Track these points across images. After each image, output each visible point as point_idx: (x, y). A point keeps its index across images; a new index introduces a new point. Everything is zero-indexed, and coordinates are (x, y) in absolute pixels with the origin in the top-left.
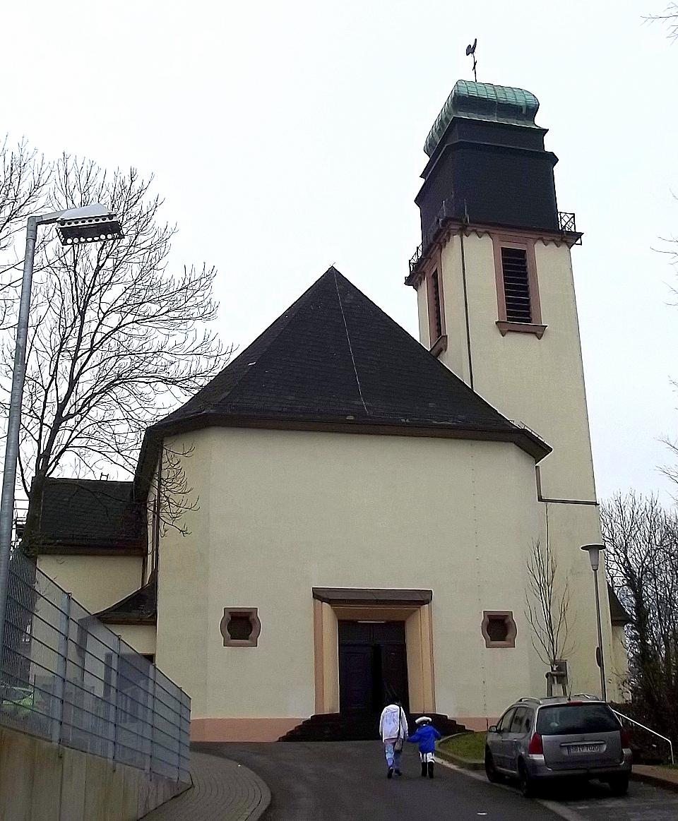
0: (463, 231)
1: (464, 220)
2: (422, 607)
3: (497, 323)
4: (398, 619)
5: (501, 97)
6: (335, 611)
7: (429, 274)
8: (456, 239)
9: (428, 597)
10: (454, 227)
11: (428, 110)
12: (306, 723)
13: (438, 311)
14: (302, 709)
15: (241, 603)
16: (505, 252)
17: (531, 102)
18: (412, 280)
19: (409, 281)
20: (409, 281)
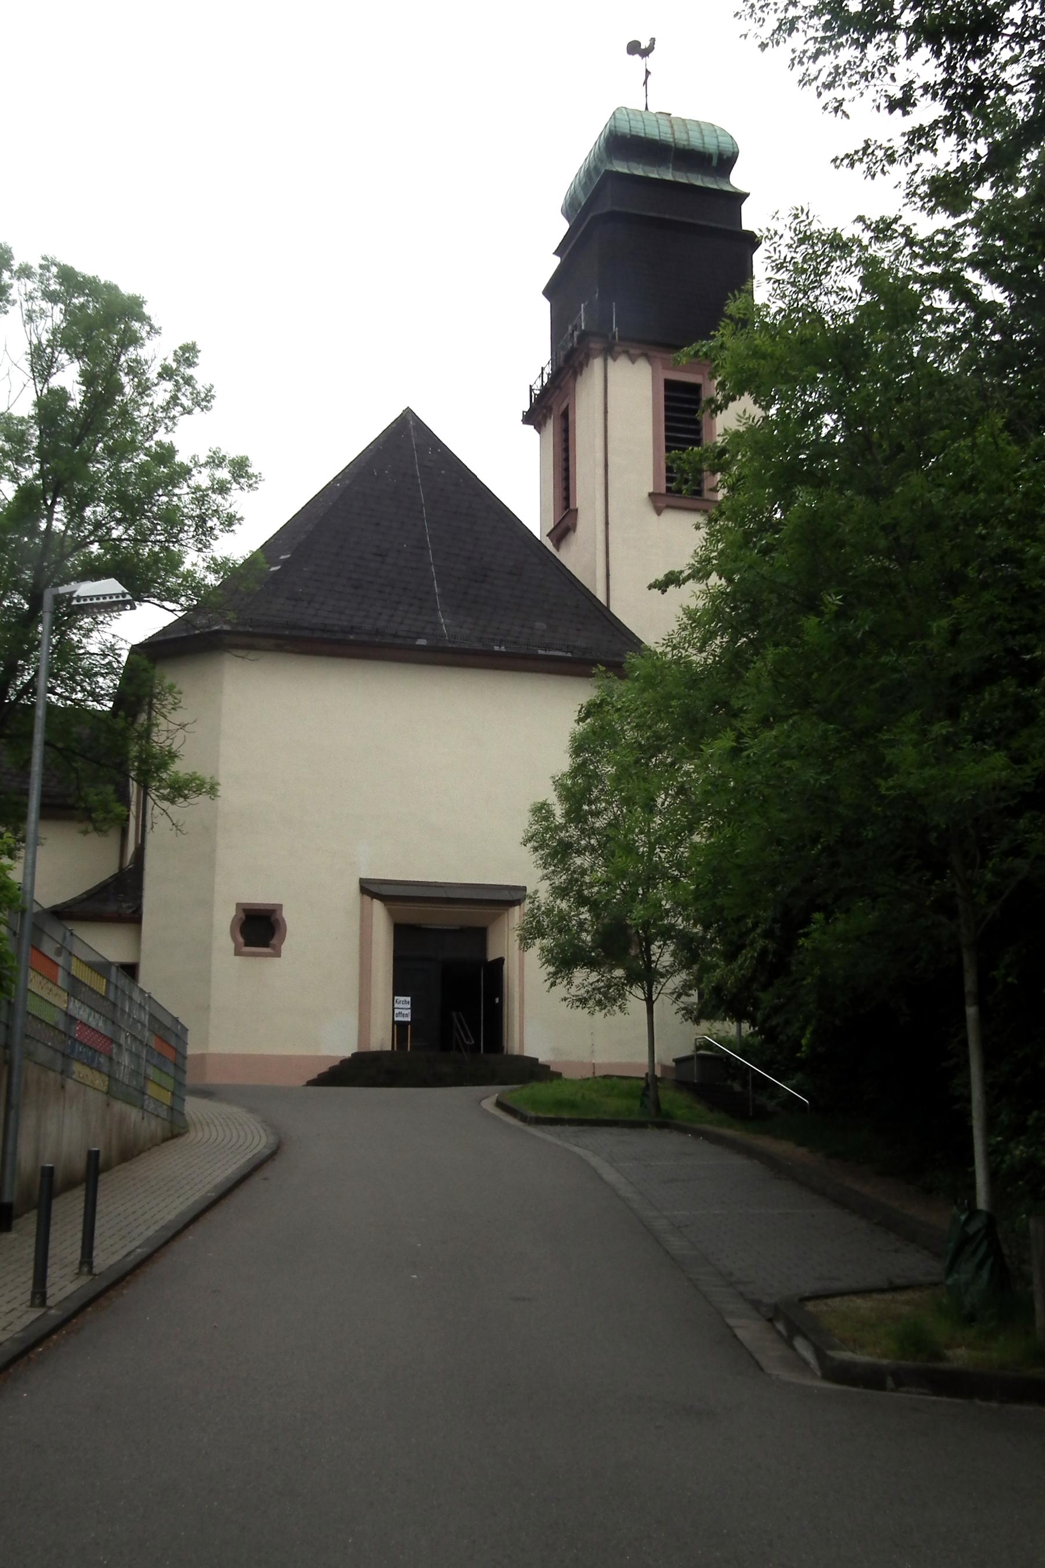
0: (609, 352)
1: (610, 335)
2: (511, 910)
3: (650, 495)
4: (480, 925)
5: (681, 138)
6: (391, 913)
7: (557, 411)
8: (597, 364)
9: (517, 896)
10: (595, 345)
11: (566, 157)
12: (344, 1062)
13: (567, 470)
14: (341, 1045)
15: (260, 897)
16: (669, 385)
17: (726, 146)
18: (533, 417)
19: (528, 418)
20: (528, 418)
